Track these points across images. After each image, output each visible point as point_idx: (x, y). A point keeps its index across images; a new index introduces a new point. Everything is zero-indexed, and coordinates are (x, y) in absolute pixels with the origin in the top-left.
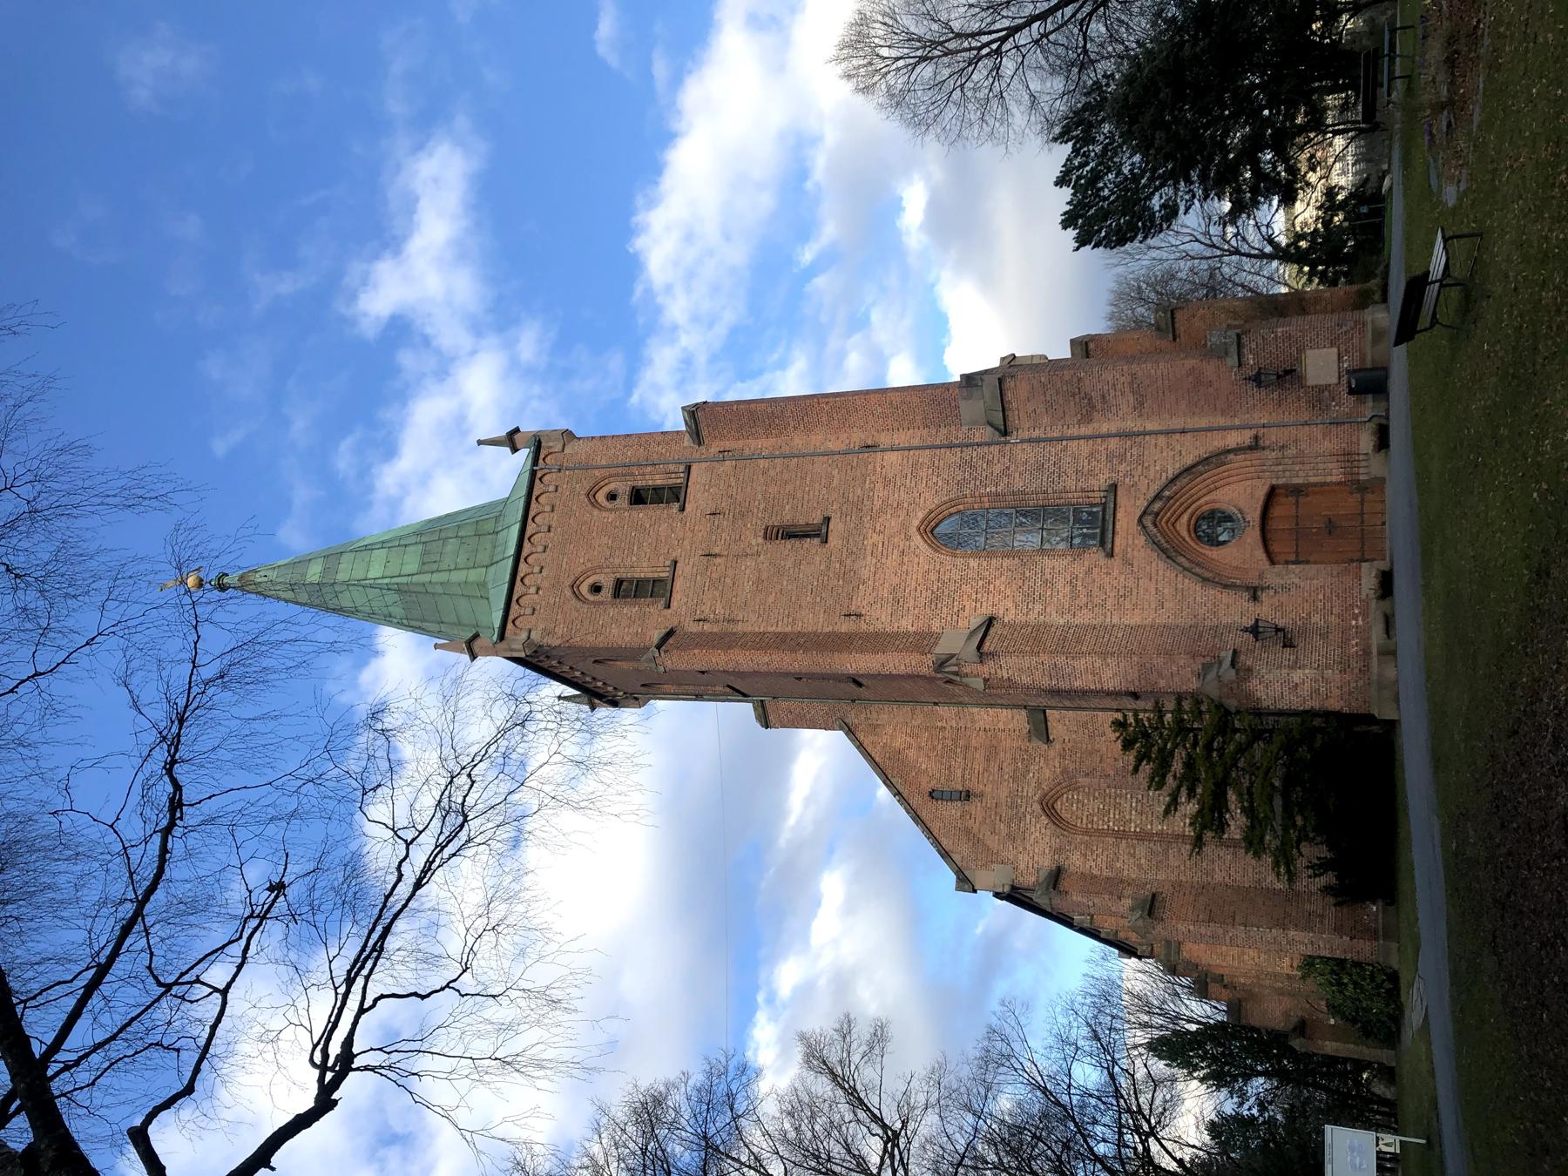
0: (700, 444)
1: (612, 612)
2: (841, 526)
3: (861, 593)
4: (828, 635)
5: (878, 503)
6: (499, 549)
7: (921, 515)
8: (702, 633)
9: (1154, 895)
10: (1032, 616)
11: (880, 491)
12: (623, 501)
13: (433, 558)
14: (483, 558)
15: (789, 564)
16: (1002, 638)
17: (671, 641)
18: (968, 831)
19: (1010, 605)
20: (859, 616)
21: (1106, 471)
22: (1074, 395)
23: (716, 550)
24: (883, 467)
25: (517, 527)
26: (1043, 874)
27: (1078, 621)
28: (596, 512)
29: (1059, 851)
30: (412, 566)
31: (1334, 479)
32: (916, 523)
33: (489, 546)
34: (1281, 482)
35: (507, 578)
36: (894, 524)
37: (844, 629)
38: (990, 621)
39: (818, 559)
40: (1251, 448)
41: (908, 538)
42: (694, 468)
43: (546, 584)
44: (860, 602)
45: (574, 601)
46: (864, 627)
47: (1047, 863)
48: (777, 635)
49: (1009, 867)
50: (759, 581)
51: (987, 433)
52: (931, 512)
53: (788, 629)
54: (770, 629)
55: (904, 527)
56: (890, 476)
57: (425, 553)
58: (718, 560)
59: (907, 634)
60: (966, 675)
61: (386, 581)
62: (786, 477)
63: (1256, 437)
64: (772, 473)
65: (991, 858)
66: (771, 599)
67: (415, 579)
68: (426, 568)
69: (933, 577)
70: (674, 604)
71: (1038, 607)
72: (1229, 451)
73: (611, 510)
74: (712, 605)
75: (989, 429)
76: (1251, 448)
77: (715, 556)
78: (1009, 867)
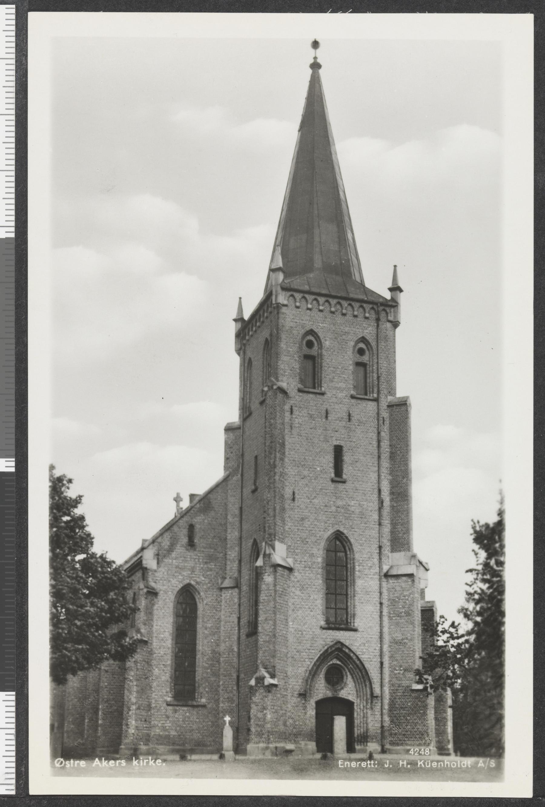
12: (306, 350)
34: (355, 707)
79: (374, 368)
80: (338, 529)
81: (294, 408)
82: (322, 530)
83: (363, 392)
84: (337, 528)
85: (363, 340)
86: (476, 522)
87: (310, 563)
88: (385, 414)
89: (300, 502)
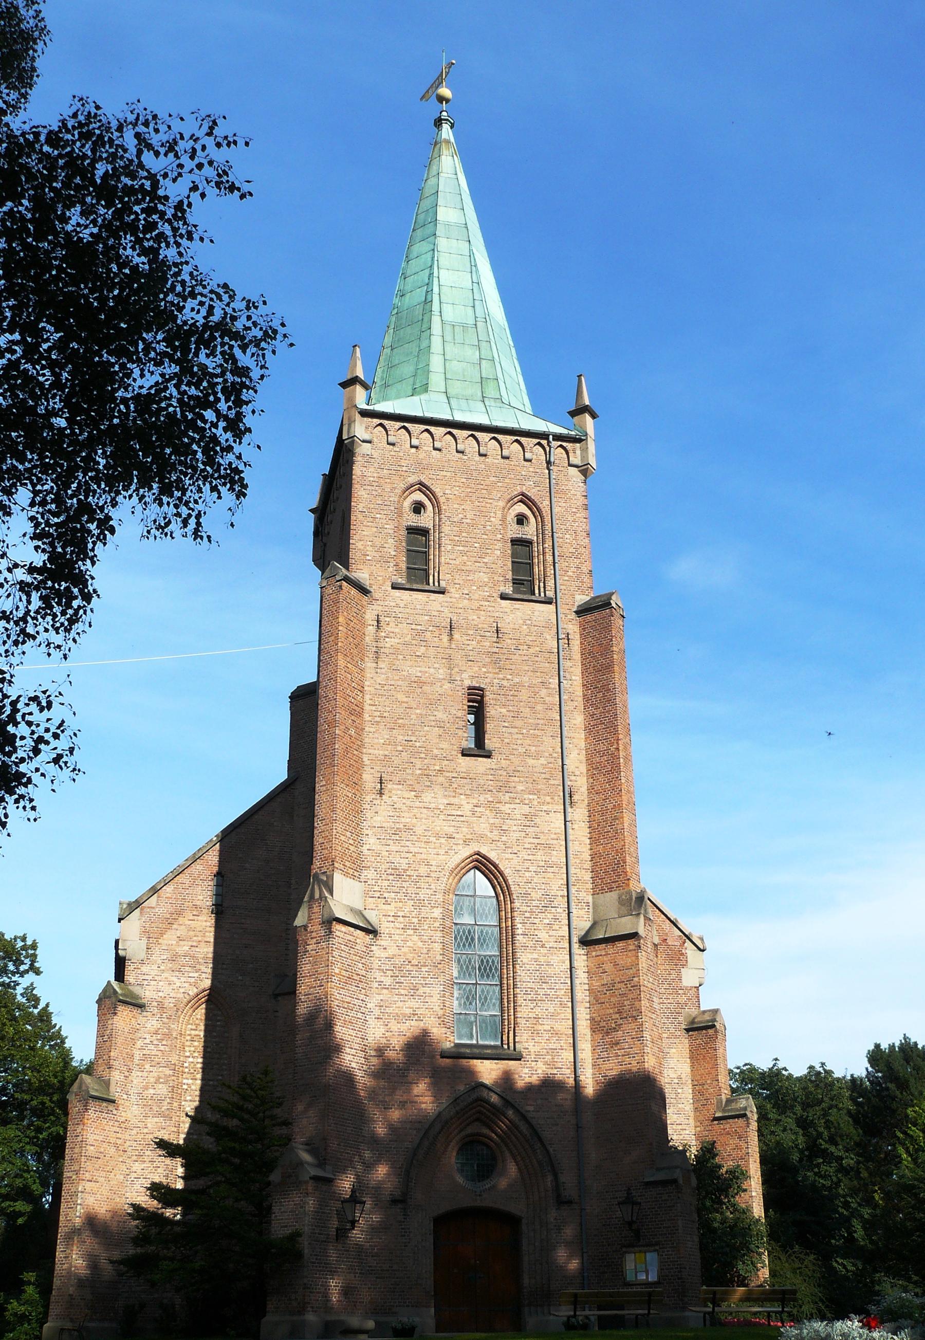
0: (577, 612)
1: (390, 527)
2: (481, 769)
3: (406, 795)
4: (359, 760)
5: (506, 808)
6: (463, 403)
7: (492, 856)
8: (364, 625)
9: (114, 1101)
10: (378, 975)
11: (521, 810)
12: (515, 531)
13: (459, 338)
14: (455, 388)
15: (440, 715)
16: (351, 945)
17: (354, 592)
18: (180, 913)
19: (392, 951)
20: (381, 793)
21: (537, 1049)
22: (619, 1012)
23: (456, 636)
24: (547, 812)
25: (484, 420)
26: (137, 990)
27: (372, 1022)
28: (501, 504)
29: (161, 1006)
30: (450, 314)
31: (526, 1281)
32: (484, 851)
33: (469, 392)
34: (524, 1227)
35: (428, 415)
36: (482, 826)
37: (365, 776)
38: (371, 931)
39: (445, 745)
40: (559, 1196)
41: (466, 842)
42: (552, 607)
43: (422, 455)
44: (395, 792)
45: (403, 486)
46: (368, 798)
47: (147, 994)
48: (360, 706)
49: (143, 955)
50: (420, 683)
51: (582, 922)
52: (496, 866)
53: (366, 717)
54: (367, 697)
55: (481, 837)
56: (538, 821)
57: (464, 327)
58: (445, 638)
59: (359, 843)
60: (310, 907)
61: (436, 289)
62: (539, 707)
63: (570, 1202)
64: (543, 692)
65: (151, 936)
66: (401, 697)
67: (436, 320)
68: (448, 328)
69: (423, 870)
70: (397, 593)
71: (388, 981)
72: (556, 1176)
73: (504, 519)
74: (396, 635)
75: (588, 925)
76: (559, 1196)
77: (451, 635)
78: (143, 955)
79: (546, 545)
80: (477, 850)
81: (381, 618)
82: (442, 852)
83: (741, 1122)
84: (474, 847)
85: (525, 499)
86: (122, 121)
87: (415, 920)
88: (572, 627)
89: (395, 798)
